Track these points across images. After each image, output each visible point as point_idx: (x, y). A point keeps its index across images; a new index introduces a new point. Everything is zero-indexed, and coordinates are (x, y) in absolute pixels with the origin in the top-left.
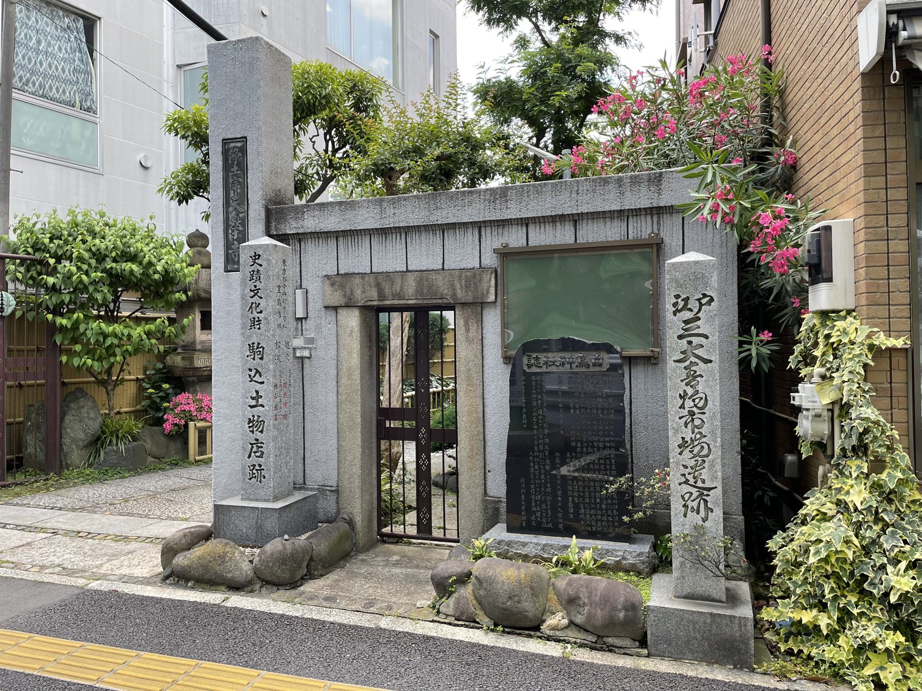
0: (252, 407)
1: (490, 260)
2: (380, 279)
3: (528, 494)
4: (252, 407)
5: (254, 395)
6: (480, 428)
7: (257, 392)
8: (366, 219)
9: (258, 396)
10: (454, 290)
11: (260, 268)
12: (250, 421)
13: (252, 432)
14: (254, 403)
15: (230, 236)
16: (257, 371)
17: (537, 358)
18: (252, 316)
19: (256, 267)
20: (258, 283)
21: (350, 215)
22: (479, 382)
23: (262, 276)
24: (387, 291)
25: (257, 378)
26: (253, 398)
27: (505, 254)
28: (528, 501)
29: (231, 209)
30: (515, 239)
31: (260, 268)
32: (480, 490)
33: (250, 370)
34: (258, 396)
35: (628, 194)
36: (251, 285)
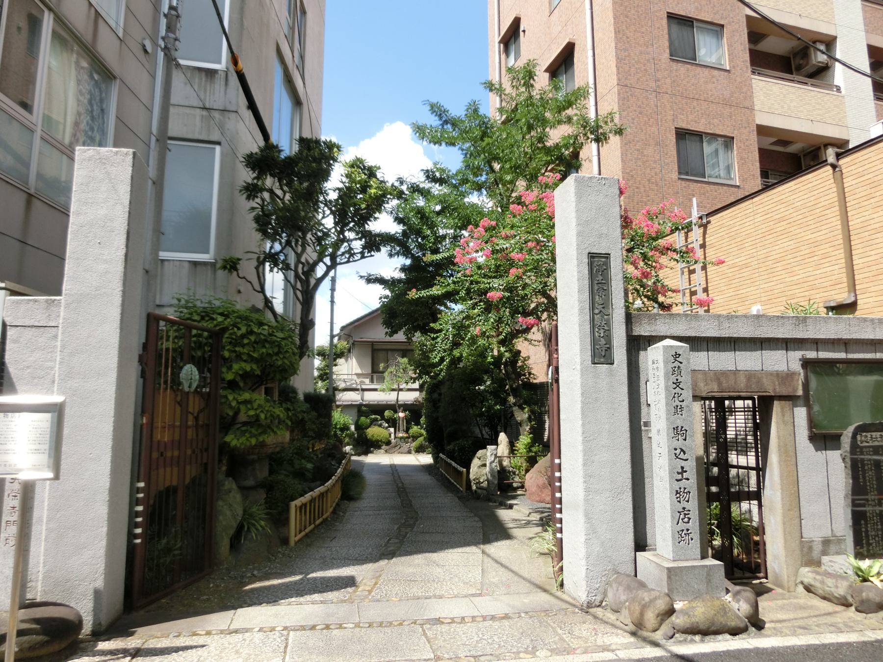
0: (678, 480)
1: (796, 367)
2: (719, 376)
3: (867, 531)
4: (678, 480)
5: (680, 471)
6: (796, 489)
7: (682, 468)
8: (708, 329)
9: (683, 471)
10: (775, 385)
11: (680, 365)
12: (677, 492)
13: (679, 502)
14: (680, 477)
15: (597, 334)
16: (682, 450)
17: (866, 436)
18: (675, 404)
19: (677, 364)
20: (679, 377)
21: (694, 324)
22: (793, 454)
23: (683, 372)
24: (725, 385)
25: (682, 456)
26: (678, 473)
27: (807, 364)
28: (867, 536)
29: (596, 311)
30: (811, 355)
31: (680, 365)
32: (798, 534)
33: (676, 449)
34: (683, 471)
35: (878, 329)
36: (673, 378)
